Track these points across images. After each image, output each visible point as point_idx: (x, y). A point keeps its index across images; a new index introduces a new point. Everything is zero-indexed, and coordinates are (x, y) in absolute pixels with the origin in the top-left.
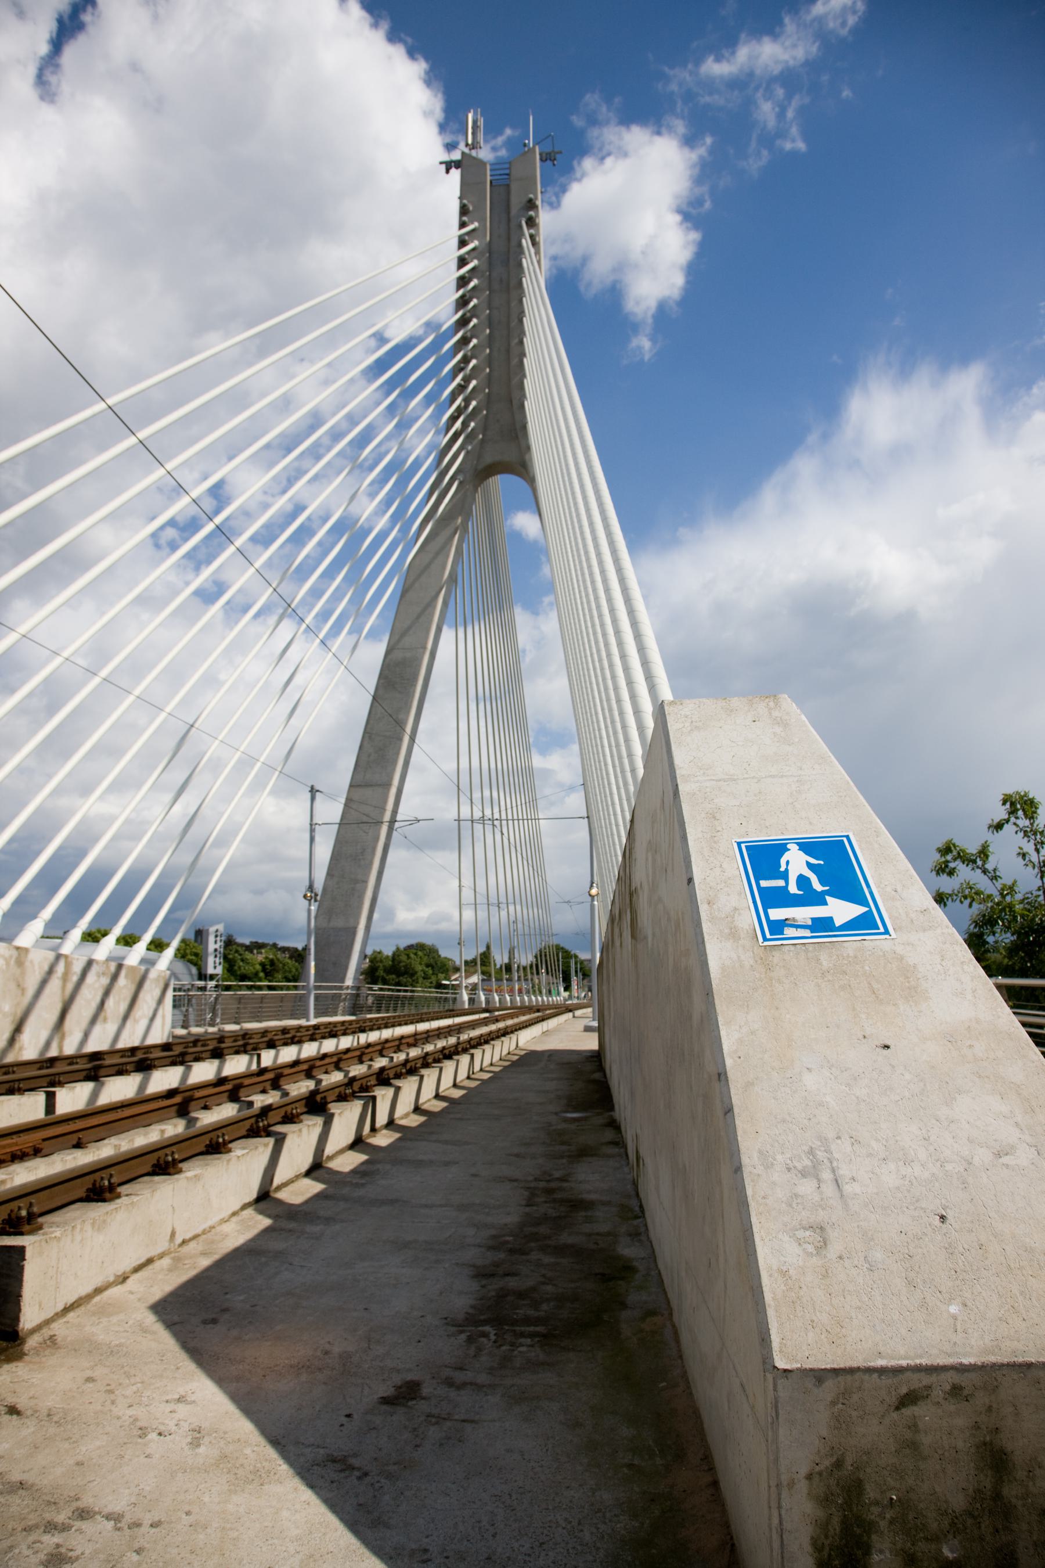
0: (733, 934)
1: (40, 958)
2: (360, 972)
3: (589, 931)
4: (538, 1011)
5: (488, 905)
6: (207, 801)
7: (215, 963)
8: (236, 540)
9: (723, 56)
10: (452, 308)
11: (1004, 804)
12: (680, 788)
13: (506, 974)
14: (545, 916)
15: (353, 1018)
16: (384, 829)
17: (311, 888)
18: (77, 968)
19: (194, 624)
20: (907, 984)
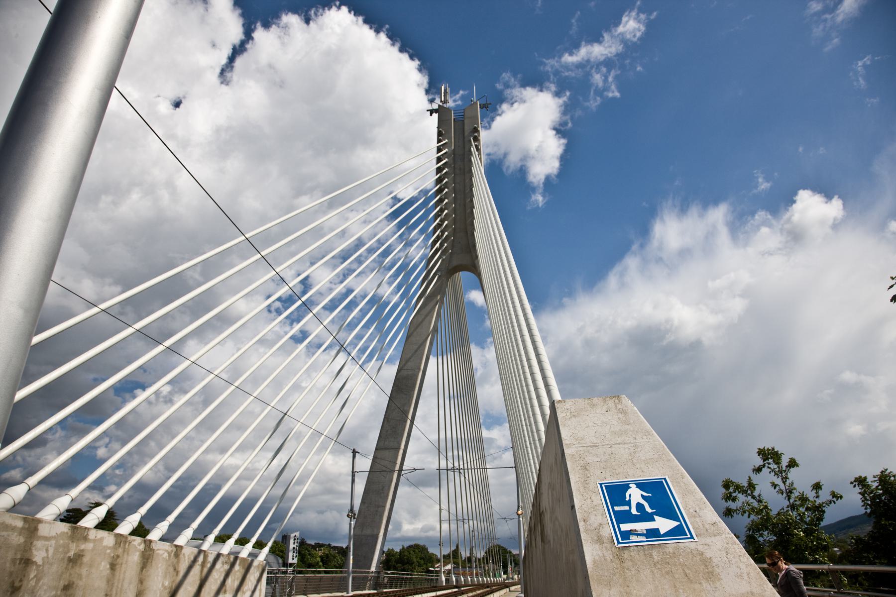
0: (599, 540)
1: (189, 553)
2: (380, 562)
3: (518, 537)
4: (488, 587)
5: (457, 520)
6: (292, 458)
7: (293, 556)
8: (314, 309)
9: (574, 53)
10: (433, 184)
11: (759, 455)
12: (565, 451)
13: (468, 564)
14: (491, 527)
15: (375, 591)
16: (395, 475)
17: (352, 510)
18: (211, 558)
19: (289, 355)
20: (707, 570)
